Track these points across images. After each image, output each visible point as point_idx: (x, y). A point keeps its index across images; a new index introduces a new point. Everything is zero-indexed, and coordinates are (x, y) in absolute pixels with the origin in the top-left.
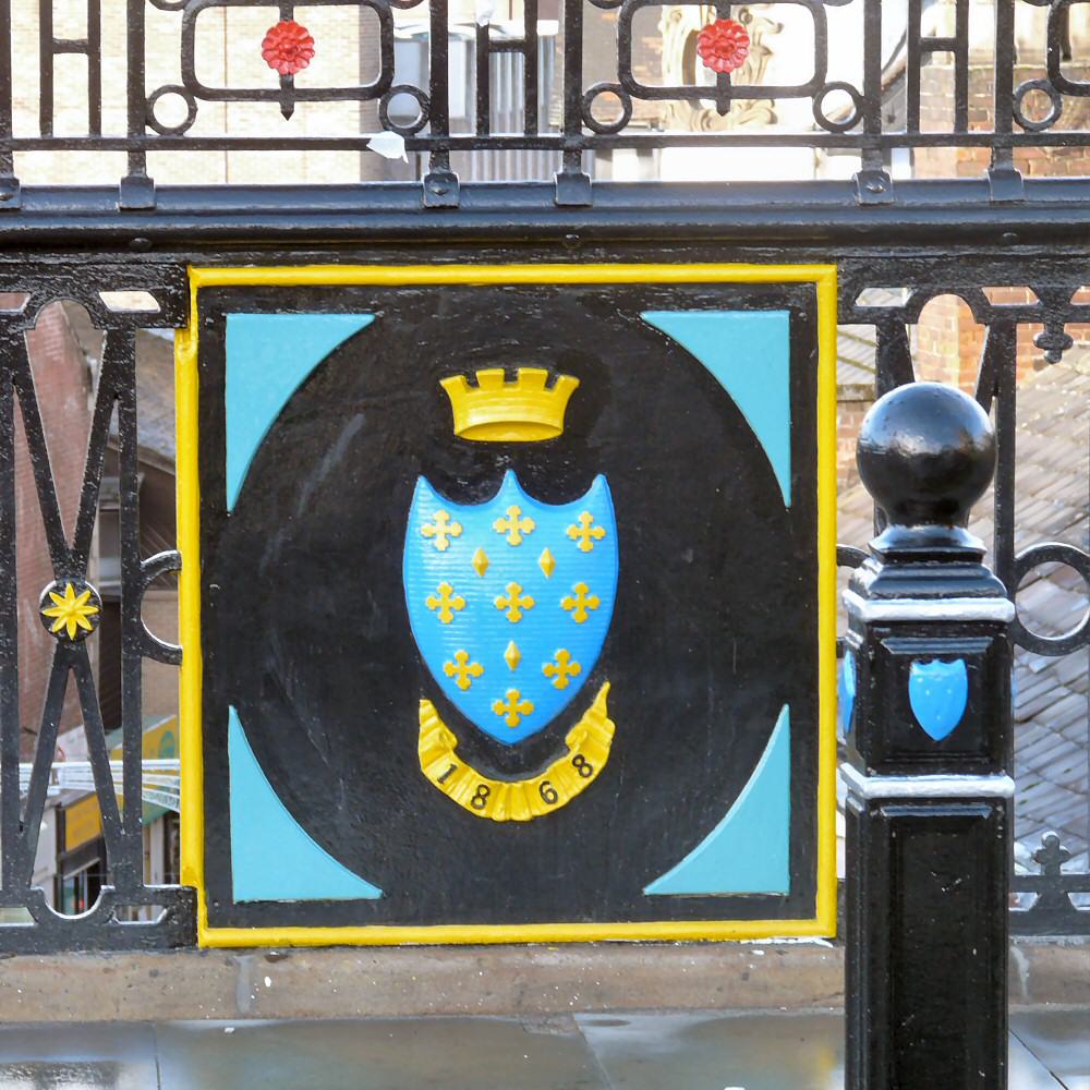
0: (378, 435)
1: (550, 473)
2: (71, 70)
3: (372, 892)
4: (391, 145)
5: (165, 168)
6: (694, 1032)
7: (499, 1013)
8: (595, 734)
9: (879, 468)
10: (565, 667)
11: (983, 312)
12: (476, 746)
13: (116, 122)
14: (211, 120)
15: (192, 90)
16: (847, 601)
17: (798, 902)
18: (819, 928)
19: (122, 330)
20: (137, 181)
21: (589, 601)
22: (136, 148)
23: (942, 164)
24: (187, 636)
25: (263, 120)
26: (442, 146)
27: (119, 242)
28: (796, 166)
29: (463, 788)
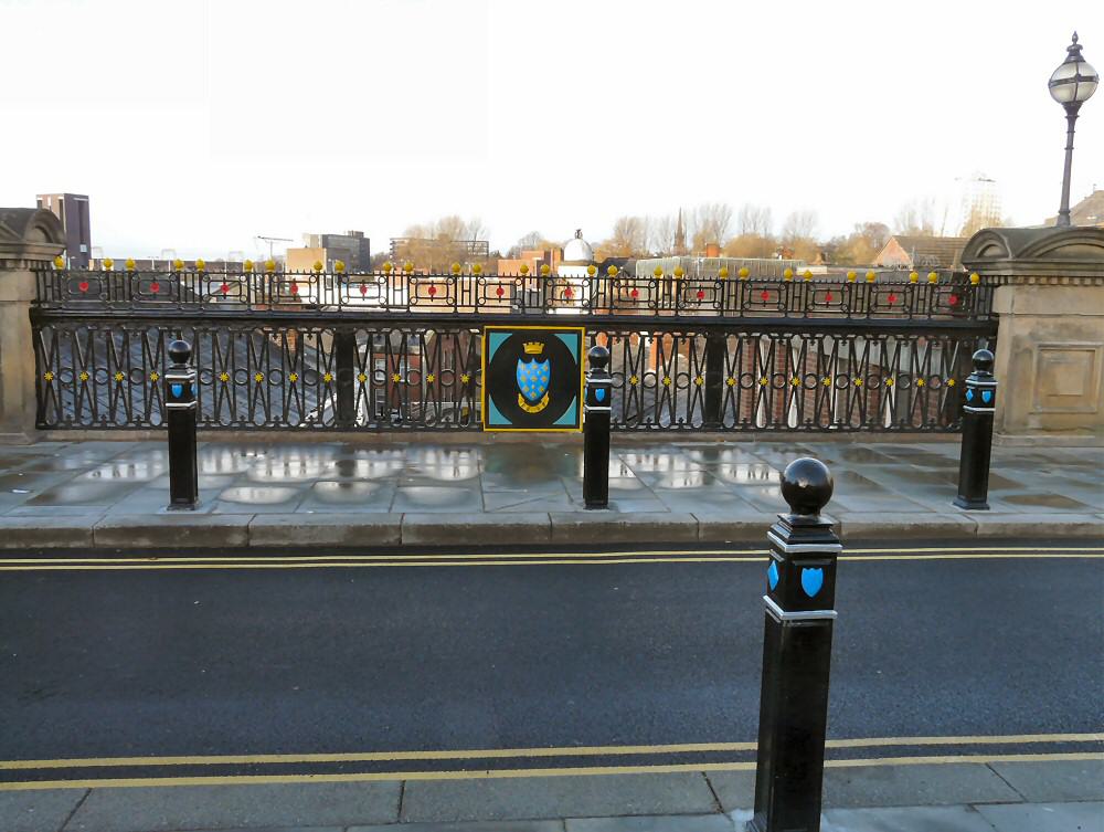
0: (512, 353)
1: (540, 359)
2: (796, 301)
3: (510, 423)
4: (516, 307)
5: (481, 310)
6: (560, 446)
7: (78, 441)
8: (546, 400)
9: (591, 359)
10: (541, 389)
11: (607, 335)
12: (527, 401)
13: (473, 303)
14: (421, 302)
15: (485, 298)
16: (586, 379)
17: (577, 426)
18: (580, 430)
19: (371, 334)
20: (476, 312)
21: (545, 379)
22: (476, 307)
23: (600, 312)
24: (483, 384)
25: (429, 302)
26: (524, 308)
27: (473, 322)
28: (577, 312)
29: (525, 408)
